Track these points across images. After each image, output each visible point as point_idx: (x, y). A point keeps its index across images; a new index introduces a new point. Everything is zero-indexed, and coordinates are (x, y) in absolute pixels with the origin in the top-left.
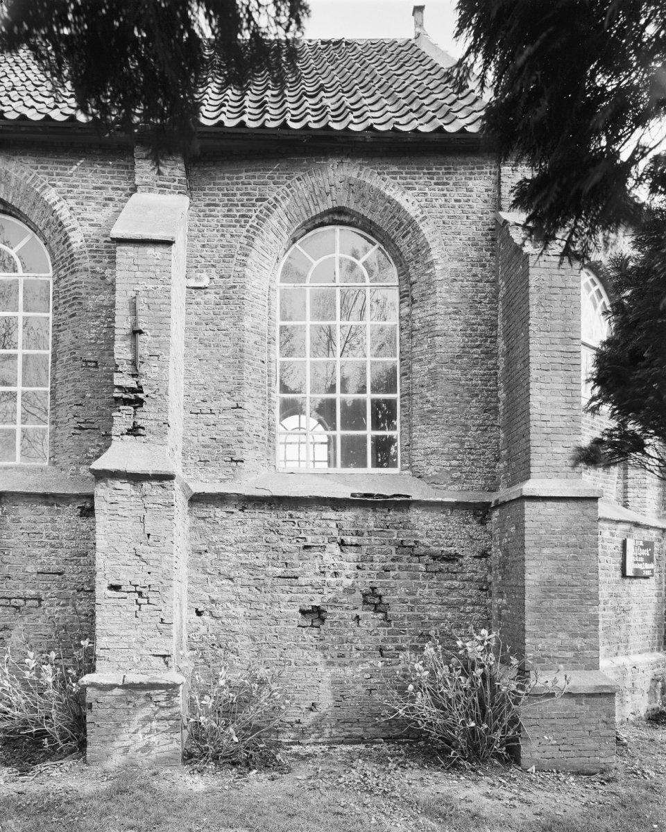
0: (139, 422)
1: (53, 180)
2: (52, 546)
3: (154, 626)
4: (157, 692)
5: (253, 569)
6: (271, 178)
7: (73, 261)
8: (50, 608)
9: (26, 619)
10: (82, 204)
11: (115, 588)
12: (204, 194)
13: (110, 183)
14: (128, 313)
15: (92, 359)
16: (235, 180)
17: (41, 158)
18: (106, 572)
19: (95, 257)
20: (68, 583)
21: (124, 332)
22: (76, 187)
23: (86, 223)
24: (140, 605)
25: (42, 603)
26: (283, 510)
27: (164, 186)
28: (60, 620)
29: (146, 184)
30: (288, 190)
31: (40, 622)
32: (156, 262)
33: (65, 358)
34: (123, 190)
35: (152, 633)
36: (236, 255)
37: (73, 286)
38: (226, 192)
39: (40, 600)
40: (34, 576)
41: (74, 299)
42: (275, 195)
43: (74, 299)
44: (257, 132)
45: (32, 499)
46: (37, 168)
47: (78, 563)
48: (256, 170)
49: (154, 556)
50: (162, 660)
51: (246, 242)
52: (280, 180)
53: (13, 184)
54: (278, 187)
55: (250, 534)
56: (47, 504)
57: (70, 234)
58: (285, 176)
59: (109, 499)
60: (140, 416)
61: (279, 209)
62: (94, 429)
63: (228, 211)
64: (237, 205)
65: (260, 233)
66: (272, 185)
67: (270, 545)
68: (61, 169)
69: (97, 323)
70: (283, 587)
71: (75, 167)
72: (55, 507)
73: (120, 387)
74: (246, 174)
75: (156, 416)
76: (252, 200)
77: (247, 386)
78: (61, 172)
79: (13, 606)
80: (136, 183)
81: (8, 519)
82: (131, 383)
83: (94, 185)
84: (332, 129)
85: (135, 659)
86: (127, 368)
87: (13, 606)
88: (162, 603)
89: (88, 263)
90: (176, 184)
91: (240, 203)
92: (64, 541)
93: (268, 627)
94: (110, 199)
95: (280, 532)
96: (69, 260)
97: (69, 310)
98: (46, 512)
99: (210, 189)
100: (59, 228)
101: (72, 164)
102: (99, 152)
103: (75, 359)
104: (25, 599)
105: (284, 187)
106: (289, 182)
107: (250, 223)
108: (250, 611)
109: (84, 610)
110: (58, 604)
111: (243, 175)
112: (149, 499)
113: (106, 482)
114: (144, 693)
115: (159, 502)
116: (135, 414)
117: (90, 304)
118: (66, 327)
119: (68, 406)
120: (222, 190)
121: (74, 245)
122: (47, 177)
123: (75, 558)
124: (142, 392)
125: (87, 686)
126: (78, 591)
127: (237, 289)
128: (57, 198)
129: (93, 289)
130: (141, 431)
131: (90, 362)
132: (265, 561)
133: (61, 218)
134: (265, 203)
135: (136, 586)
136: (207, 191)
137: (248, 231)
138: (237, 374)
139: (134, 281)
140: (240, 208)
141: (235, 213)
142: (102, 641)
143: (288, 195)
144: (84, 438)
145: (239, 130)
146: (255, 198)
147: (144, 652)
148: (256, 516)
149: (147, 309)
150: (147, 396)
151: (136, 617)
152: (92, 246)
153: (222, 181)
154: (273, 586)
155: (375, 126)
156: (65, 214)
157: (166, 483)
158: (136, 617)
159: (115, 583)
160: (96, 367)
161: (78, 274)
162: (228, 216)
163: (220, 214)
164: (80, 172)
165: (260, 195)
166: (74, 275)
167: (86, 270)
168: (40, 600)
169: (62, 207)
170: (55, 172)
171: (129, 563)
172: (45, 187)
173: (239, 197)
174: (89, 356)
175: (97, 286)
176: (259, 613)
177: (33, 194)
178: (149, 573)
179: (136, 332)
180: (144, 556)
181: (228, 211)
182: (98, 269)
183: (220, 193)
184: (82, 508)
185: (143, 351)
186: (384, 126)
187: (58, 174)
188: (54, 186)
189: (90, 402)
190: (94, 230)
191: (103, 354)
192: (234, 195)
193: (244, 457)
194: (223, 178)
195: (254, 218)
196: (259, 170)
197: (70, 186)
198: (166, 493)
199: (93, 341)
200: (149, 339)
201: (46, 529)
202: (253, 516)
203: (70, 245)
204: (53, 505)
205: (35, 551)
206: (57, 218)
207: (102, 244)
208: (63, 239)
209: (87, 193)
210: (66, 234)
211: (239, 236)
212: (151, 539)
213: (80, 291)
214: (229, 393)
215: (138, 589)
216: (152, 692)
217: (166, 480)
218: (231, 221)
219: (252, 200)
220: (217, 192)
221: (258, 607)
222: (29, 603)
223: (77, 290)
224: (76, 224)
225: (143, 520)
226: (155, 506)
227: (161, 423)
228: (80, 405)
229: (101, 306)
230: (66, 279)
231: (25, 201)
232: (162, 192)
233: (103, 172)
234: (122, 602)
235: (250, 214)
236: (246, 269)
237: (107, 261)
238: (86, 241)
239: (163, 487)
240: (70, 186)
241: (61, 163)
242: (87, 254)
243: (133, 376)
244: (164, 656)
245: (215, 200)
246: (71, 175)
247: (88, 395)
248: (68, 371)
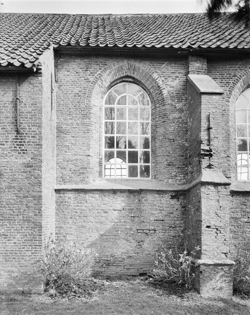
0: (211, 163)
1: (156, 70)
2: (160, 210)
3: (222, 242)
4: (225, 267)
5: (236, 219)
6: (238, 68)
7: (164, 101)
8: (159, 234)
9: (150, 238)
10: (167, 79)
11: (208, 227)
12: (212, 74)
13: (177, 71)
14: (206, 121)
15: (172, 138)
16: (224, 69)
17: (152, 62)
18: (206, 221)
19: (172, 99)
20: (166, 224)
21: (204, 128)
22: (165, 72)
23: (168, 86)
24: (217, 233)
25: (156, 232)
26: (248, 196)
27: (199, 72)
28: (163, 238)
29: (193, 71)
30: (245, 72)
31: (155, 239)
32: (216, 101)
33: (161, 138)
34: (182, 73)
35: (221, 244)
36: (225, 98)
37: (164, 111)
38: (220, 73)
39: (155, 231)
40: (153, 221)
41: (164, 115)
42: (240, 74)
43: (164, 115)
44: (242, 50)
45: (152, 192)
46: (150, 66)
47: (170, 217)
48: (233, 65)
49: (223, 215)
50: (224, 254)
51: (229, 93)
52: (243, 68)
53: (141, 71)
54: (241, 71)
55: (235, 206)
56: (158, 194)
57: (163, 91)
58: (244, 67)
59: (206, 193)
60: (212, 161)
61: (241, 80)
62: (173, 165)
63: (222, 81)
64: (225, 78)
65: (234, 89)
66: (239, 70)
67: (243, 210)
68: (159, 66)
69: (174, 125)
70: (247, 226)
71: (164, 65)
72: (161, 195)
73: (203, 150)
74: (229, 66)
75: (218, 161)
76: (231, 76)
77: (231, 148)
78: (159, 67)
79: (145, 233)
80: (189, 70)
81: (143, 199)
82: (207, 148)
83: (171, 71)
84: (118, 46)
85: (215, 254)
86: (206, 142)
87: (145, 233)
88: (225, 233)
89: (170, 102)
90: (203, 70)
91: (226, 77)
92: (164, 208)
93: (242, 242)
94: (177, 77)
95: (246, 205)
96: (162, 100)
97: (162, 120)
98: (158, 197)
99: (214, 72)
100: (158, 88)
101: (163, 64)
102: (173, 59)
103: (166, 138)
104: (149, 230)
105: (243, 71)
106: (246, 69)
107: (230, 85)
108: (235, 235)
109: (172, 235)
110: (162, 232)
111: (228, 66)
112: (221, 193)
113: (205, 186)
114: (221, 267)
115: (224, 194)
116: (210, 160)
117: (171, 117)
118: (161, 126)
119: (163, 157)
120: (219, 72)
121: (164, 95)
122: (154, 69)
123: (169, 214)
124: (212, 151)
125: (201, 264)
126: (170, 227)
127: (226, 111)
128: (157, 77)
129: (172, 111)
130: (212, 167)
131: (171, 139)
132: (241, 216)
133: (159, 85)
134: (236, 78)
135: (216, 226)
136: (213, 73)
137: (229, 88)
138: (227, 144)
139: (208, 109)
140: (226, 79)
141: (224, 81)
142: (204, 247)
143: (245, 74)
144: (170, 169)
145: (152, 48)
146: (232, 75)
147: (219, 251)
148: (237, 199)
149: (213, 119)
150: (214, 153)
151: (216, 238)
152: (171, 95)
153: (219, 69)
154: (243, 226)
155: (201, 46)
156: (160, 83)
157: (227, 187)
158: (216, 238)
159: (209, 225)
160: (174, 141)
161: (166, 106)
162: (221, 83)
163: (218, 82)
164: (166, 67)
165: (234, 74)
166: (164, 106)
167: (169, 104)
168: (155, 231)
169: (159, 80)
170: (157, 67)
171: (214, 217)
172: (153, 73)
173: (225, 75)
174: (171, 137)
175: (173, 110)
176: (238, 236)
177: (149, 75)
178: (221, 221)
179: (209, 129)
180: (219, 215)
181: (222, 81)
182: (173, 104)
183: (218, 74)
184: (171, 195)
185: (212, 136)
186: (149, 45)
187: (158, 68)
188: (156, 72)
189: (172, 155)
190: (171, 89)
191: (176, 137)
192: (224, 74)
193: (231, 176)
194: (220, 68)
195: (231, 83)
196: (234, 65)
197: (163, 72)
198: (227, 191)
199: (172, 132)
200: (214, 131)
201: (158, 203)
202: (236, 199)
203: (163, 95)
204: (160, 194)
205: (154, 212)
206: (157, 85)
207: (175, 94)
208: (159, 92)
209: (169, 75)
210: (161, 90)
211: (226, 90)
212: (222, 209)
213: (167, 112)
214: (224, 151)
215: (217, 227)
216: (223, 267)
217: (227, 185)
218: (223, 85)
219: (231, 76)
220: (217, 73)
221: (238, 234)
222: (151, 232)
223: (165, 112)
224: (165, 87)
225: (218, 201)
226: (223, 195)
227: (219, 163)
228: (168, 156)
229: (175, 118)
230: (160, 108)
231: (144, 78)
232: (198, 74)
233: (175, 67)
234: (211, 232)
235: (230, 82)
236: (229, 103)
237: (177, 101)
238: (169, 93)
239: (226, 188)
240: (163, 72)
241: (159, 63)
242: (169, 98)
243: (208, 145)
244: (225, 253)
245: (216, 76)
246: (163, 68)
247: (171, 152)
248: (163, 143)
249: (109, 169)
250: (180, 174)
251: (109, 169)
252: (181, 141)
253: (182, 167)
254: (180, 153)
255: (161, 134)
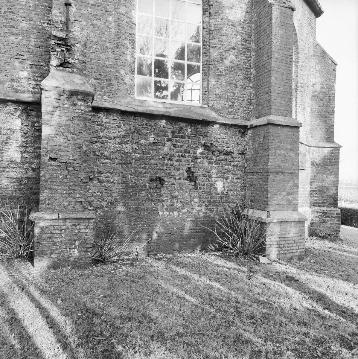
199: (24, 3)
249: (194, 90)
250: (36, 76)
251: (194, 90)
252: (39, 21)
253: (39, 65)
254: (37, 41)
255: (4, 4)
